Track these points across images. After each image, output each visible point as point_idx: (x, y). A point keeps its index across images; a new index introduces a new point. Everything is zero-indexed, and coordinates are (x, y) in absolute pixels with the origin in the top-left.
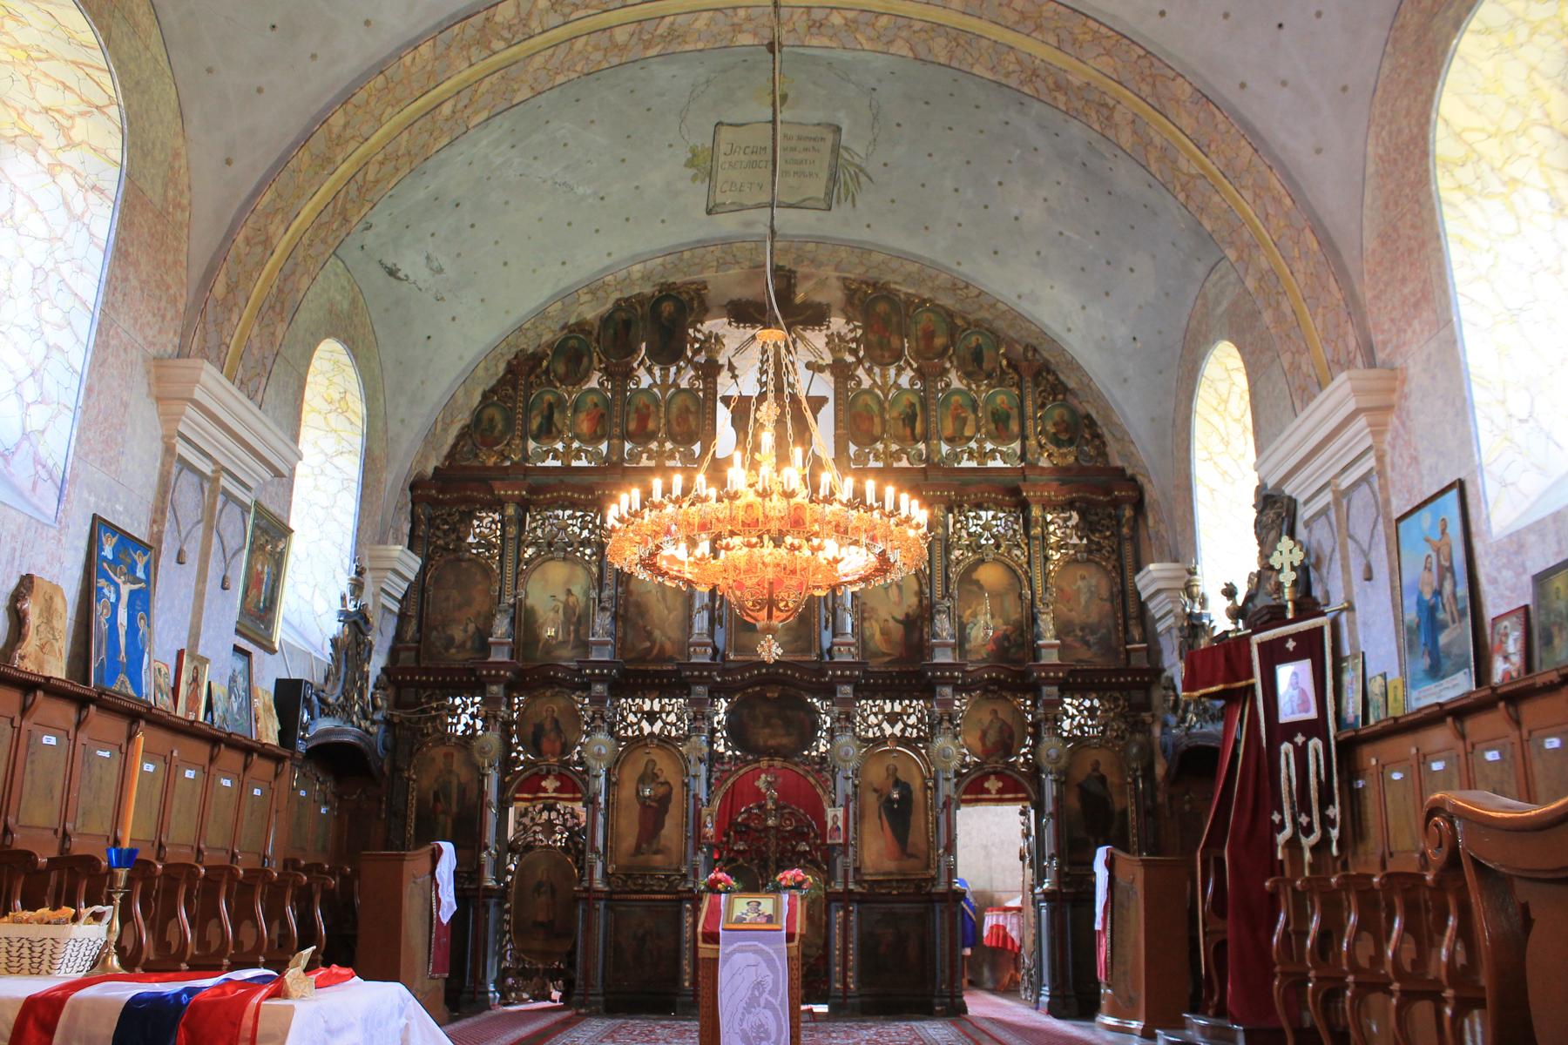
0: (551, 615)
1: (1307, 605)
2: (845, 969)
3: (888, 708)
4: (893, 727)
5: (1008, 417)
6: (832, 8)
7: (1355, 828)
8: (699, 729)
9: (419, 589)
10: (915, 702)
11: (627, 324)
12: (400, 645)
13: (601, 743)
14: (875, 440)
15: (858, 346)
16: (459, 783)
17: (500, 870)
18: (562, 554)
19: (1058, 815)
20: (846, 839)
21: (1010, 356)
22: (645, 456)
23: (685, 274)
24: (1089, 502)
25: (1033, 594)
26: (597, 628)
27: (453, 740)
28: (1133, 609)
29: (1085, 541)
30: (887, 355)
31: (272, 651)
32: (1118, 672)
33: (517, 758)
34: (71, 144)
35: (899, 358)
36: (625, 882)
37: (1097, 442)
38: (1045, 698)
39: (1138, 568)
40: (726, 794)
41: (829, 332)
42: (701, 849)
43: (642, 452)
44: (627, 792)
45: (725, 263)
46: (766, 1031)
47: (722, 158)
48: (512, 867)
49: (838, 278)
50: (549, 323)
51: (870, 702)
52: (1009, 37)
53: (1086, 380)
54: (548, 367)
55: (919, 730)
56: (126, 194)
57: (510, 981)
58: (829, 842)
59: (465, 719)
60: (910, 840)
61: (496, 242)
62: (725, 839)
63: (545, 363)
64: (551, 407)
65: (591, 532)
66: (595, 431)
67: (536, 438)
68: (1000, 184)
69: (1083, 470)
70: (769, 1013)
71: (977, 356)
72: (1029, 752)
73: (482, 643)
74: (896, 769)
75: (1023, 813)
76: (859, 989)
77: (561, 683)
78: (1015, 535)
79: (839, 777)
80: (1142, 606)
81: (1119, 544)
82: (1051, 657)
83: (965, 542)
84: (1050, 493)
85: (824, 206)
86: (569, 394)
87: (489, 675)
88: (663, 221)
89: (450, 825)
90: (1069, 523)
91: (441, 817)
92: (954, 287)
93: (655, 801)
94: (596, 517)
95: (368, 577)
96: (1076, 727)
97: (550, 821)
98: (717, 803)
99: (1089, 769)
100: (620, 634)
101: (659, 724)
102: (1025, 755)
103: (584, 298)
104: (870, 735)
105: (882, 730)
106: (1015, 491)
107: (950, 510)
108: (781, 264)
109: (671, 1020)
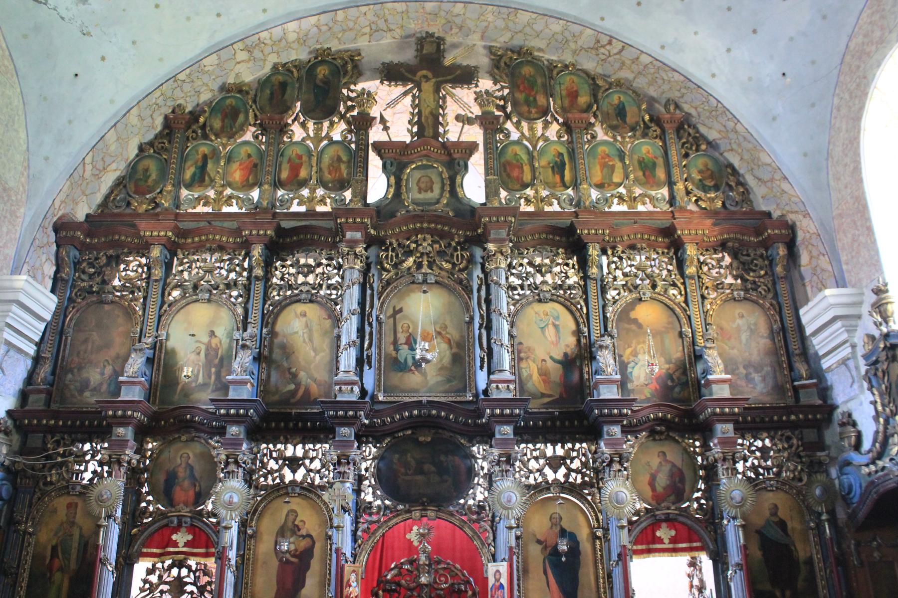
0: (193, 357)
4: (555, 472)
5: (654, 165)
13: (233, 490)
14: (526, 186)
16: (81, 536)
18: (207, 296)
22: (296, 202)
32: (788, 410)
43: (293, 199)
44: (264, 546)
51: (530, 446)
59: (93, 466)
65: (240, 274)
66: (248, 180)
71: (621, 112)
81: (774, 284)
86: (224, 146)
89: (66, 584)
91: (58, 576)
93: (294, 556)
98: (363, 558)
100: (264, 376)
101: (301, 472)
102: (698, 500)
107: (604, 252)
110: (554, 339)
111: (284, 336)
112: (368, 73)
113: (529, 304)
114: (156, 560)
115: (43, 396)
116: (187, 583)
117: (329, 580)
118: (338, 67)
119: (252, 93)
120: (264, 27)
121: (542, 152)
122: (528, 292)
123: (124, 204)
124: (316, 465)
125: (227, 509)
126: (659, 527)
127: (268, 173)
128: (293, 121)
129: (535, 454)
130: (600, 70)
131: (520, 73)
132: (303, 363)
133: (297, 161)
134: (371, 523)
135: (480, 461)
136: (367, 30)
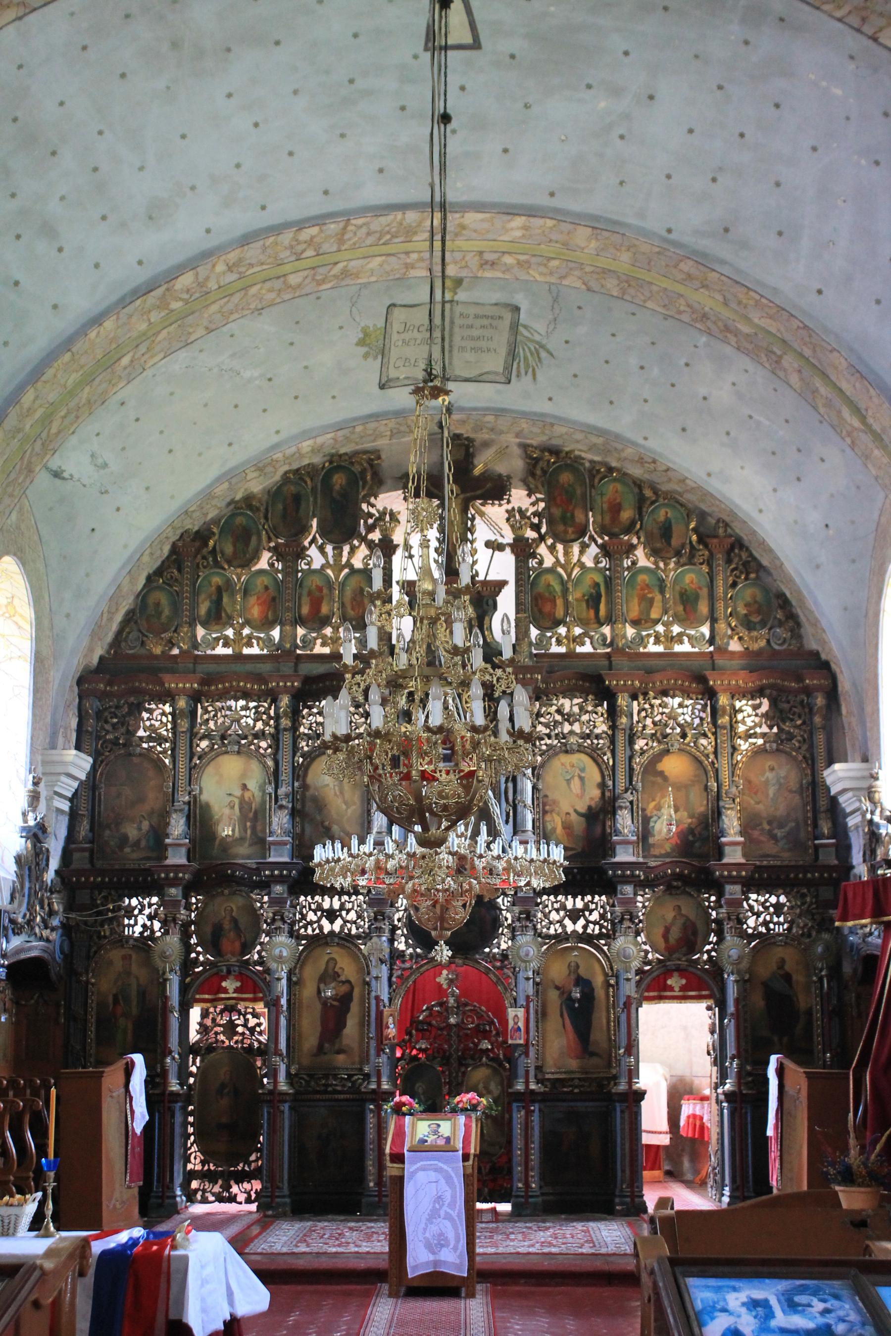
0: (227, 811)
2: (527, 1169)
3: (569, 904)
4: (574, 923)
5: (697, 597)
6: (504, 253)
10: (597, 898)
11: (297, 499)
12: (73, 846)
13: (282, 944)
14: (558, 623)
15: (540, 522)
16: (139, 985)
18: (236, 748)
19: (737, 1016)
20: (527, 1040)
21: (702, 529)
22: (319, 641)
23: (357, 443)
24: (781, 690)
25: (719, 787)
26: (275, 826)
27: (131, 942)
28: (823, 803)
29: (775, 730)
30: (570, 530)
32: (805, 869)
33: (197, 958)
35: (583, 534)
37: (791, 623)
38: (727, 897)
41: (509, 507)
42: (383, 1050)
43: (315, 639)
44: (308, 991)
45: (399, 432)
47: (395, 337)
48: (194, 1069)
50: (214, 502)
51: (552, 897)
52: (680, 288)
53: (777, 562)
54: (214, 547)
55: (601, 927)
58: (510, 1042)
59: (142, 919)
60: (592, 1037)
61: (161, 432)
62: (407, 1037)
63: (211, 543)
65: (266, 724)
66: (266, 617)
67: (204, 625)
68: (687, 365)
69: (775, 654)
70: (448, 1223)
71: (666, 531)
72: (713, 949)
74: (578, 966)
75: (709, 1008)
76: (541, 1187)
77: (240, 882)
81: (811, 734)
82: (734, 856)
84: (741, 680)
86: (238, 577)
88: (334, 397)
89: (130, 1026)
90: (759, 711)
91: (122, 1021)
92: (641, 461)
93: (335, 1000)
94: (270, 708)
96: (763, 924)
98: (398, 1002)
99: (774, 966)
100: (298, 830)
101: (339, 922)
102: (708, 952)
103: (251, 475)
104: (552, 931)
105: (564, 927)
106: (701, 679)
107: (634, 697)
108: (457, 432)
109: (357, 1221)
110: (579, 791)
111: (316, 789)
112: (389, 482)
113: (556, 754)
114: (208, 1005)
115: (87, 854)
116: (238, 1025)
117: (369, 1021)
118: (355, 475)
119: (262, 509)
120: (275, 447)
121: (578, 581)
122: (556, 742)
123: (138, 643)
124: (352, 916)
125: (278, 962)
126: (671, 976)
127: (288, 609)
128: (310, 544)
129: (556, 906)
130: (647, 476)
131: (558, 481)
132: (335, 816)
133: (317, 594)
134: (404, 969)
135: (504, 912)
136: (389, 433)
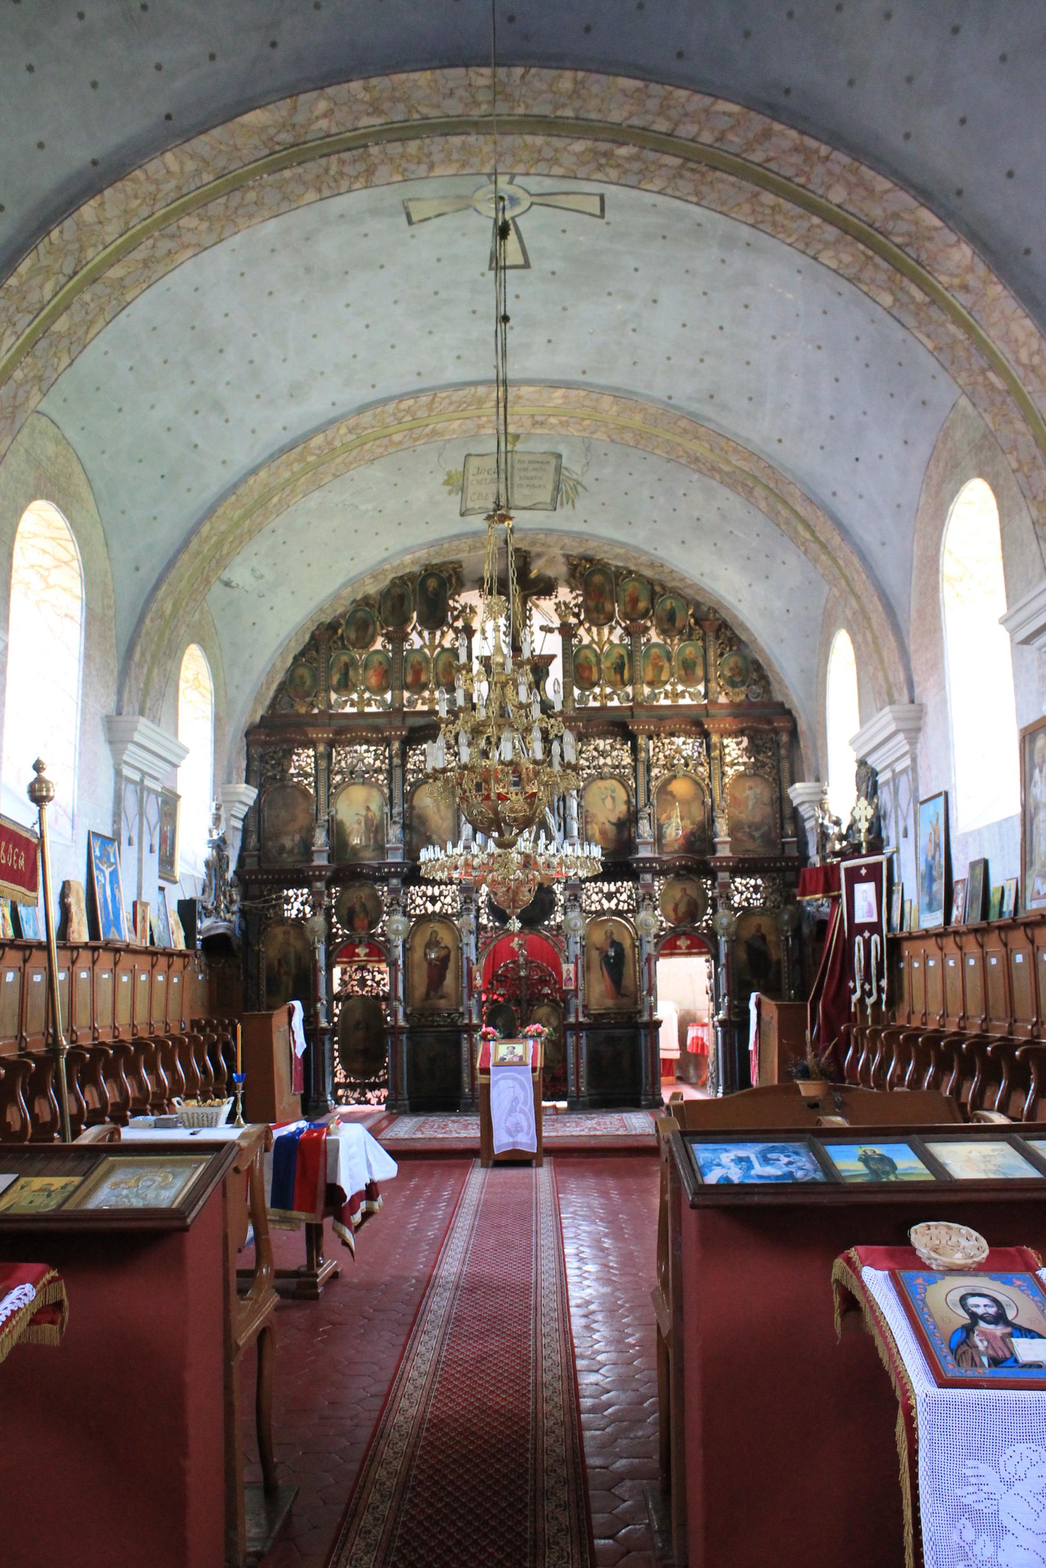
0: (356, 826)
1: (876, 845)
2: (578, 1077)
5: (695, 664)
7: (895, 996)
8: (468, 910)
9: (257, 810)
10: (625, 883)
11: (401, 598)
13: (397, 921)
15: (580, 611)
17: (330, 1015)
18: (361, 780)
19: (728, 966)
20: (576, 987)
21: (697, 614)
22: (420, 701)
24: (757, 731)
28: (787, 812)
29: (753, 760)
30: (602, 617)
31: (175, 882)
32: (775, 860)
34: (49, 586)
36: (419, 1020)
37: (763, 682)
39: (792, 782)
40: (489, 955)
41: (557, 601)
44: (418, 955)
46: (521, 1127)
47: (471, 477)
49: (564, 555)
51: (593, 884)
52: (678, 440)
55: (629, 904)
56: (87, 618)
57: (340, 1092)
59: (297, 905)
61: (302, 551)
64: (346, 666)
66: (381, 684)
67: (336, 691)
68: (685, 495)
69: (752, 705)
70: (522, 1116)
71: (671, 617)
73: (307, 844)
74: (612, 933)
77: (367, 877)
78: (699, 756)
79: (571, 941)
80: (795, 810)
81: (779, 762)
82: (724, 852)
83: (662, 762)
84: (728, 724)
85: (550, 507)
87: (314, 875)
91: (284, 978)
92: (652, 565)
95: (222, 812)
97: (363, 977)
98: (483, 961)
99: (753, 930)
100: (407, 839)
102: (706, 921)
103: (368, 581)
104: (593, 908)
105: (602, 905)
106: (698, 724)
107: (650, 738)
